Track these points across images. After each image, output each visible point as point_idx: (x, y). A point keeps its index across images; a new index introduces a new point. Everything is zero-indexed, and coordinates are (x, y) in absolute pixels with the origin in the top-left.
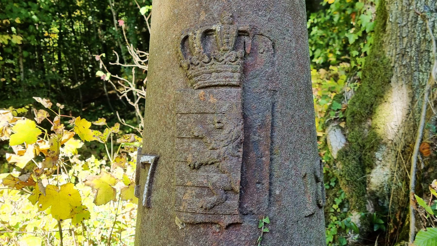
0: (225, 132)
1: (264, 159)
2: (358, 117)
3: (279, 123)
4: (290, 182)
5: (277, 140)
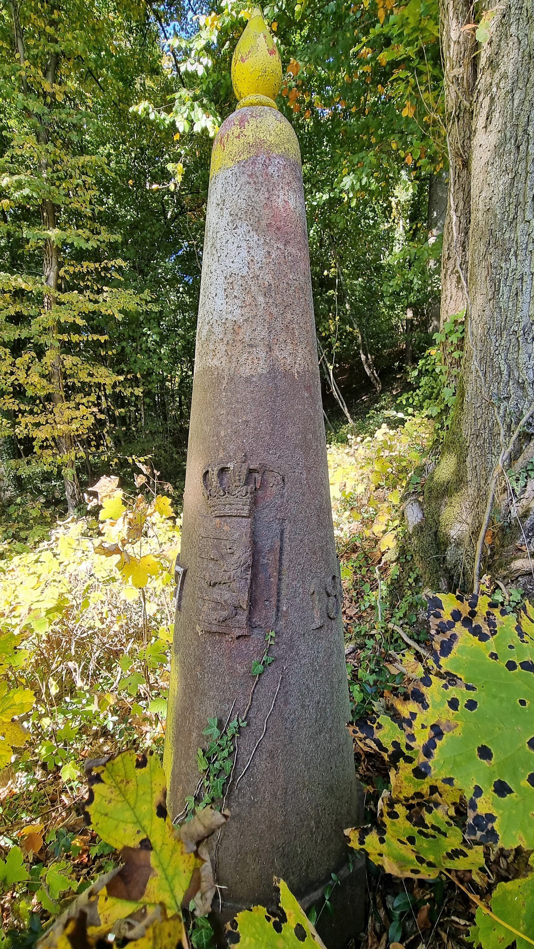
0: (236, 557)
1: (272, 579)
2: (434, 494)
3: (287, 548)
4: (298, 599)
5: (285, 563)
